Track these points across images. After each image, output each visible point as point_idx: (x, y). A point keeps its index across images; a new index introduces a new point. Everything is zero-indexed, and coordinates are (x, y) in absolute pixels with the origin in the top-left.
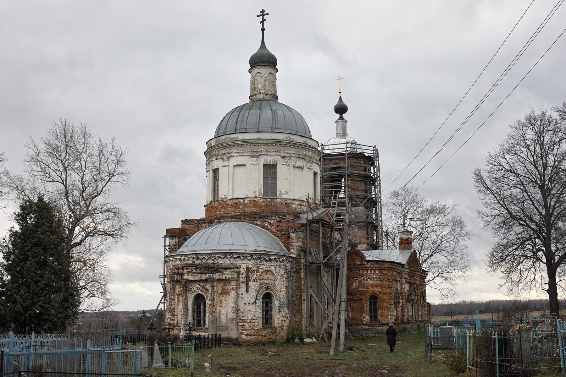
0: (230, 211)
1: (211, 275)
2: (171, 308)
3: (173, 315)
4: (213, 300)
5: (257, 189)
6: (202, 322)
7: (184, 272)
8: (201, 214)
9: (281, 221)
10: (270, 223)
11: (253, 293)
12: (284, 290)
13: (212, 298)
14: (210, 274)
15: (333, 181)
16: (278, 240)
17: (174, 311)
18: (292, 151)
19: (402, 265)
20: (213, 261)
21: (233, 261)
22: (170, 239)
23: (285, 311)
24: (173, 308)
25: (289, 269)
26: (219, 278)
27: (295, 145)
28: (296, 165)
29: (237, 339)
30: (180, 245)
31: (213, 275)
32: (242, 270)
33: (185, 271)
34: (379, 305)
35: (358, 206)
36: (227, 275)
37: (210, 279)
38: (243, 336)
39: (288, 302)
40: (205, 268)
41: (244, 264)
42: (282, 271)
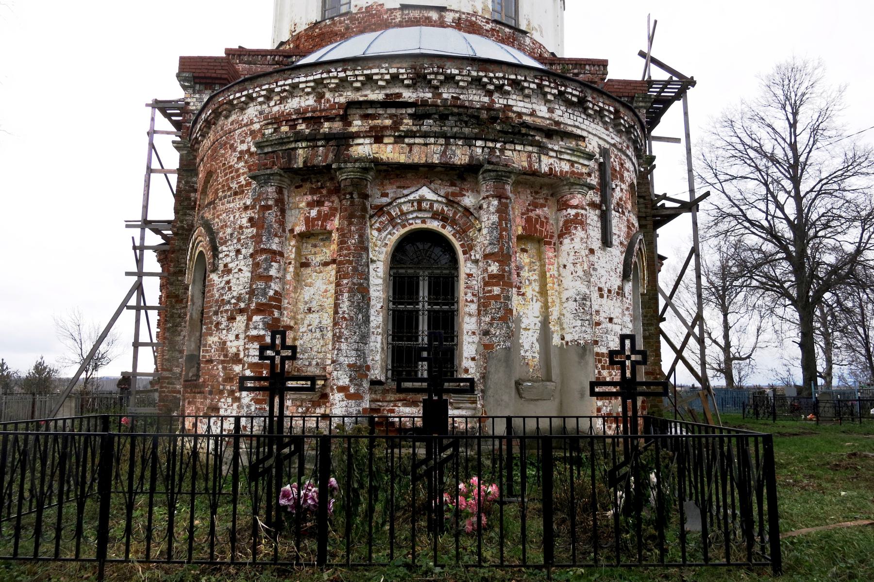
1: (492, 149)
2: (265, 294)
7: (353, 129)
13: (501, 249)
14: (490, 144)
17: (279, 308)
20: (486, 99)
22: (191, 91)
24: (276, 292)
26: (525, 164)
31: (502, 150)
37: (489, 163)
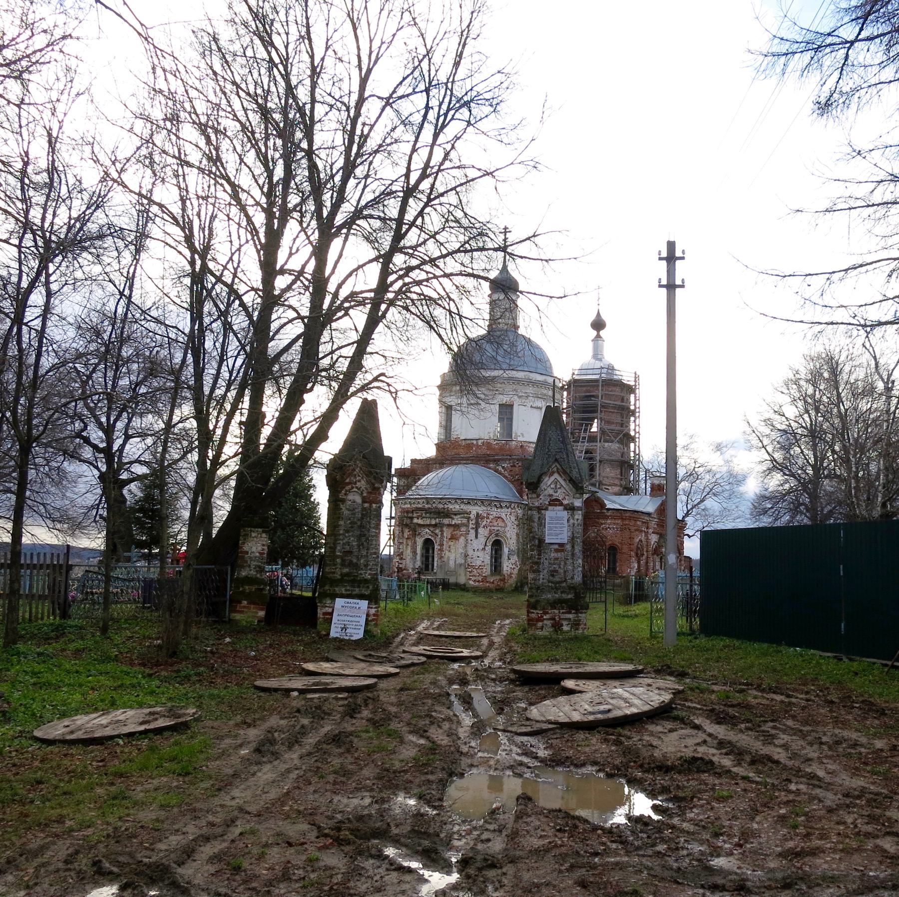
0: (463, 453)
3: (401, 559)
4: (441, 545)
5: (492, 430)
6: (430, 567)
8: (430, 451)
9: (514, 466)
10: (503, 467)
11: (482, 539)
12: (514, 537)
15: (584, 412)
16: (511, 486)
18: (530, 390)
19: (649, 514)
21: (463, 507)
23: (514, 558)
25: (521, 516)
27: (534, 383)
28: (534, 405)
29: (464, 585)
30: (409, 487)
32: (472, 516)
33: (415, 515)
34: (618, 556)
35: (612, 442)
36: (457, 520)
38: (471, 582)
39: (518, 549)
40: (435, 513)
41: (474, 510)
42: (513, 518)
